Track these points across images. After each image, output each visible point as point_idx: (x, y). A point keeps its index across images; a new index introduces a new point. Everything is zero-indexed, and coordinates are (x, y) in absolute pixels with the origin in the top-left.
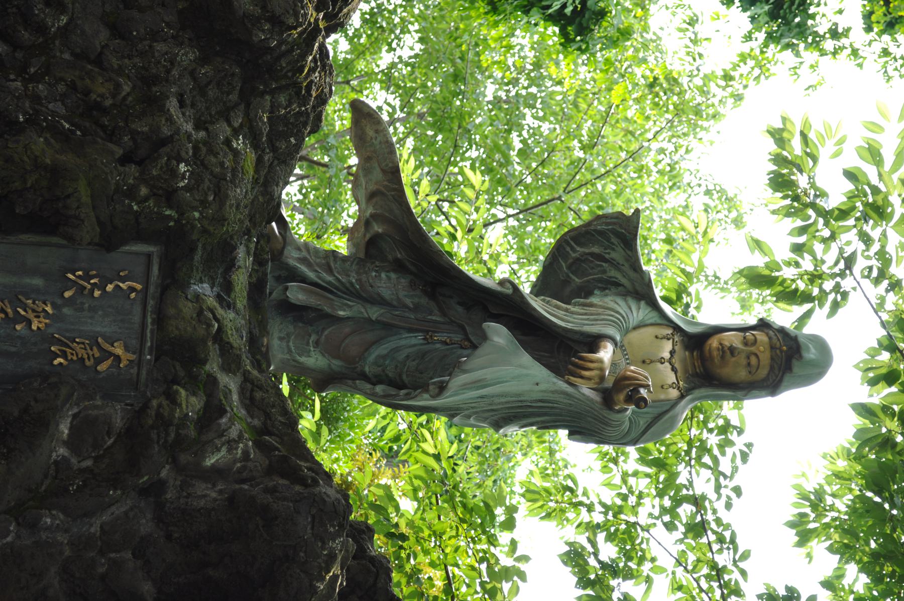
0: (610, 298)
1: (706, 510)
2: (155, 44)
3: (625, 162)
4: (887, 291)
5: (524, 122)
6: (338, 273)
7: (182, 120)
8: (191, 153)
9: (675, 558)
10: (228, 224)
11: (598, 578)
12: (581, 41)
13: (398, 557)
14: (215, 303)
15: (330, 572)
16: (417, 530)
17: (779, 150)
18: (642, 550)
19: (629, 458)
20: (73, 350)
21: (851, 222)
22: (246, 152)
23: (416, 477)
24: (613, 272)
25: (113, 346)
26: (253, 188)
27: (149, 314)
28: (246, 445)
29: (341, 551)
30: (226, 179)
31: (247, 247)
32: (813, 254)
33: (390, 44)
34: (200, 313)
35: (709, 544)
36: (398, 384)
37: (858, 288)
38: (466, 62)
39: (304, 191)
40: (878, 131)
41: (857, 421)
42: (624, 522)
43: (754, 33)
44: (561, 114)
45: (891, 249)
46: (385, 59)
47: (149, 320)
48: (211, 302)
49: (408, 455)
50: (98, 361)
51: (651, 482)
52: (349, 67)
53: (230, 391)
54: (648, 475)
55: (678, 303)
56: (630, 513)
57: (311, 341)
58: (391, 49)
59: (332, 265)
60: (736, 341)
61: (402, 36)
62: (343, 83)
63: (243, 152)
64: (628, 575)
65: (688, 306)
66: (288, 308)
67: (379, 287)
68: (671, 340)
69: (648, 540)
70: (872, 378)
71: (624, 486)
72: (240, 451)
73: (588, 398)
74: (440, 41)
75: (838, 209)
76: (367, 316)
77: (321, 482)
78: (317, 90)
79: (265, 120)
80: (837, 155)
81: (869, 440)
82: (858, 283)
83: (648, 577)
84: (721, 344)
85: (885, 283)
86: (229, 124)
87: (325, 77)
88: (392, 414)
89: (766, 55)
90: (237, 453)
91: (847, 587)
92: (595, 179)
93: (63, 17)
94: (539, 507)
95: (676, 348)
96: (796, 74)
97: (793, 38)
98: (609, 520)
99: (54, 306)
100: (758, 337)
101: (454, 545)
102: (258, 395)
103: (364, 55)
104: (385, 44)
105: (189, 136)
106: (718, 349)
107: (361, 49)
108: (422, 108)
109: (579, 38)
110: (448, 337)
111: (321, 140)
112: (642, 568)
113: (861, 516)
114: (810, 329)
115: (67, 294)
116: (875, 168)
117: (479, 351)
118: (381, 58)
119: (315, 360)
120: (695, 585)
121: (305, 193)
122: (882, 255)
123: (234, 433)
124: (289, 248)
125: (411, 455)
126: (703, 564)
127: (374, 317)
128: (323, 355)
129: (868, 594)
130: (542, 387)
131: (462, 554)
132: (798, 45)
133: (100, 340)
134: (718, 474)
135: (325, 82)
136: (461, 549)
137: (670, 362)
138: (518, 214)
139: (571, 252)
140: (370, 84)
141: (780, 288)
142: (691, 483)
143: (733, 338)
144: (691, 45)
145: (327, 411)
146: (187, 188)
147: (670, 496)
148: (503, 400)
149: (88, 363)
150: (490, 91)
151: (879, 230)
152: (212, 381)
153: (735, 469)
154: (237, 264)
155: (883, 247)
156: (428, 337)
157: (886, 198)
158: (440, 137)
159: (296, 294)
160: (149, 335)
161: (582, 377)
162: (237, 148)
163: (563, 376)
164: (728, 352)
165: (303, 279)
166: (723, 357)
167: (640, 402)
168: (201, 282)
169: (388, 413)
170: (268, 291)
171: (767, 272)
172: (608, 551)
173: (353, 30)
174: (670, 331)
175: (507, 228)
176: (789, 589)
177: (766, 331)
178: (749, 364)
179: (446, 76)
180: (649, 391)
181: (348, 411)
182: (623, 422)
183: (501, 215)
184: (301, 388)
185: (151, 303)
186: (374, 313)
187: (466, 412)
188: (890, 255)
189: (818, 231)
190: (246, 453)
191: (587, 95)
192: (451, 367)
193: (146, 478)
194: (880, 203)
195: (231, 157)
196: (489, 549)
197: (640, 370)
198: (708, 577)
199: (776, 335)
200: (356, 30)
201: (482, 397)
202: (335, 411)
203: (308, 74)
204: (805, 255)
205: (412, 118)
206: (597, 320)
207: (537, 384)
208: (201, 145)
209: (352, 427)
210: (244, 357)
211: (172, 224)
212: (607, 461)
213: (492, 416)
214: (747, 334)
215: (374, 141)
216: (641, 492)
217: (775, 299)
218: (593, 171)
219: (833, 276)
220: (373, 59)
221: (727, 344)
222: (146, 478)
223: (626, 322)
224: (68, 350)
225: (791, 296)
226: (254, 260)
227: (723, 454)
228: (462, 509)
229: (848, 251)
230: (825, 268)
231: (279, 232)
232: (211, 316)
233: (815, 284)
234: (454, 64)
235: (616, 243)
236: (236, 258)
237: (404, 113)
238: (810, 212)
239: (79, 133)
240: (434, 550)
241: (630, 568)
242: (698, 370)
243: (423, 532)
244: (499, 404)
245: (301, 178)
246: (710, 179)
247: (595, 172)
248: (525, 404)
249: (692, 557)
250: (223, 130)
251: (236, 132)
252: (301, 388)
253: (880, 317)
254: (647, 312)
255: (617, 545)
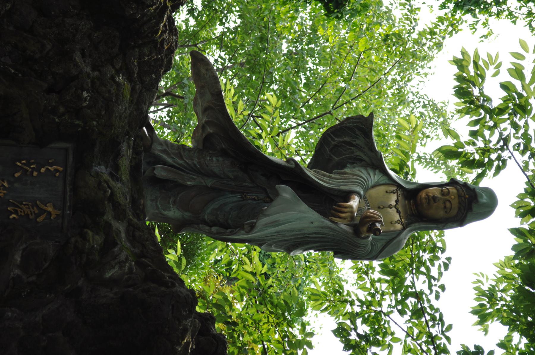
0: (357, 169)
1: (423, 301)
2: (66, 19)
3: (370, 89)
4: (530, 158)
5: (307, 66)
6: (186, 158)
7: (84, 65)
8: (90, 85)
9: (406, 332)
10: (115, 128)
11: (357, 344)
12: (338, 12)
13: (232, 337)
14: (108, 178)
15: (184, 340)
16: (244, 320)
17: (461, 73)
18: (385, 328)
19: (375, 271)
20: (21, 209)
21: (506, 116)
22: (124, 84)
23: (243, 287)
24: (358, 152)
25: (46, 206)
26: (129, 106)
27: (68, 185)
28: (131, 264)
29: (191, 326)
30: (112, 101)
31: (128, 143)
32: (483, 137)
33: (221, 21)
34: (99, 183)
35: (427, 322)
36: (225, 226)
37: (512, 157)
38: (267, 29)
39: (170, 114)
40: (521, 58)
41: (513, 240)
42: (373, 311)
43: (447, 4)
44: (330, 59)
45: (531, 132)
46: (219, 29)
47: (68, 189)
48: (106, 177)
49: (236, 274)
50: (38, 216)
51: (389, 285)
52: (196, 35)
53: (120, 231)
54: (387, 281)
55: (401, 172)
56: (377, 306)
57: (170, 201)
58: (222, 24)
59: (182, 154)
60: (437, 193)
61: (229, 15)
62: (193, 45)
63: (122, 84)
64: (377, 343)
65: (407, 173)
66: (155, 181)
67: (212, 166)
68: (396, 194)
69: (389, 322)
70: (522, 212)
71: (372, 289)
72: (127, 268)
73: (344, 230)
74: (252, 17)
75: (498, 108)
76: (205, 184)
77: (177, 285)
78: (168, 45)
79: (136, 64)
80: (496, 74)
81: (522, 251)
82: (512, 154)
83: (389, 345)
84: (427, 195)
85: (528, 153)
86: (114, 67)
87: (172, 37)
88: (226, 248)
89: (456, 17)
90: (125, 269)
91: (514, 346)
92: (351, 100)
93: (8, 5)
94: (320, 304)
95: (399, 198)
96: (474, 28)
97: (471, 6)
98: (364, 310)
99: (9, 182)
100: (450, 190)
101: (267, 328)
102: (137, 234)
103: (205, 28)
104: (218, 20)
105: (89, 75)
106: (426, 198)
107: (203, 24)
108: (242, 60)
109: (336, 10)
110: (256, 196)
111: (180, 82)
112: (386, 339)
113: (521, 302)
114: (484, 183)
115: (17, 175)
116: (519, 82)
117: (274, 203)
118: (216, 29)
119: (174, 213)
120: (419, 348)
121: (171, 116)
122: (526, 136)
123: (123, 257)
124: (155, 144)
125: (239, 274)
126: (423, 334)
127: (209, 185)
128: (178, 209)
129: (528, 350)
130: (316, 224)
131: (272, 334)
132: (475, 10)
133: (38, 202)
134: (430, 278)
135: (172, 40)
136: (271, 330)
137: (395, 207)
138: (304, 123)
139: (331, 141)
140: (210, 46)
141: (464, 159)
142: (413, 283)
143: (435, 191)
144: (408, 13)
145: (187, 250)
146: (88, 107)
147: (401, 293)
148: (292, 233)
149: (31, 217)
150: (285, 47)
151: (523, 121)
152: (108, 225)
153: (441, 274)
154: (122, 153)
155: (526, 131)
156: (243, 196)
157: (527, 101)
158: (254, 77)
159: (160, 172)
160: (68, 198)
161: (340, 217)
162: (118, 82)
163: (328, 218)
164: (432, 199)
165: (164, 163)
166: (429, 203)
167: (376, 231)
168: (99, 164)
169: (223, 248)
170: (142, 171)
171: (455, 149)
172: (363, 329)
173: (197, 12)
174: (395, 188)
175: (297, 133)
176: (477, 347)
177: (455, 186)
178: (445, 207)
179: (256, 38)
180: (382, 225)
181: (200, 250)
182: (367, 245)
183: (294, 125)
184: (170, 236)
185: (69, 178)
186: (209, 182)
187: (269, 242)
188: (531, 136)
189: (486, 122)
190: (130, 269)
191: (346, 47)
192: (257, 213)
193: (69, 286)
194: (523, 103)
195: (115, 87)
196: (288, 329)
197: (376, 212)
198: (426, 343)
199: (461, 188)
200: (199, 12)
201: (278, 232)
202: (192, 249)
203: (161, 35)
204: (479, 138)
205: (236, 66)
206: (349, 182)
207: (312, 223)
208: (96, 80)
209: (203, 260)
210: (128, 210)
211: (80, 129)
212: (361, 274)
213: (285, 244)
214: (444, 188)
215: (205, 76)
216: (383, 292)
217: (460, 165)
218: (350, 95)
219: (496, 150)
220: (211, 30)
221: (431, 195)
222: (69, 286)
223: (366, 183)
224: (19, 210)
225: (470, 164)
226: (133, 152)
227: (433, 265)
228: (270, 306)
229: (505, 134)
230: (491, 145)
231: (148, 134)
232: (106, 185)
233: (485, 156)
234: (260, 31)
235: (359, 134)
236: (120, 149)
237: (231, 63)
238: (482, 111)
239: (20, 75)
240: (255, 332)
241: (378, 340)
242: (414, 212)
243: (248, 321)
244: (289, 236)
245: (166, 106)
246: (425, 97)
247: (352, 96)
248: (305, 236)
249: (416, 331)
250: (110, 71)
251: (118, 72)
252: (170, 236)
253: (526, 175)
254: (380, 176)
255: (369, 326)
